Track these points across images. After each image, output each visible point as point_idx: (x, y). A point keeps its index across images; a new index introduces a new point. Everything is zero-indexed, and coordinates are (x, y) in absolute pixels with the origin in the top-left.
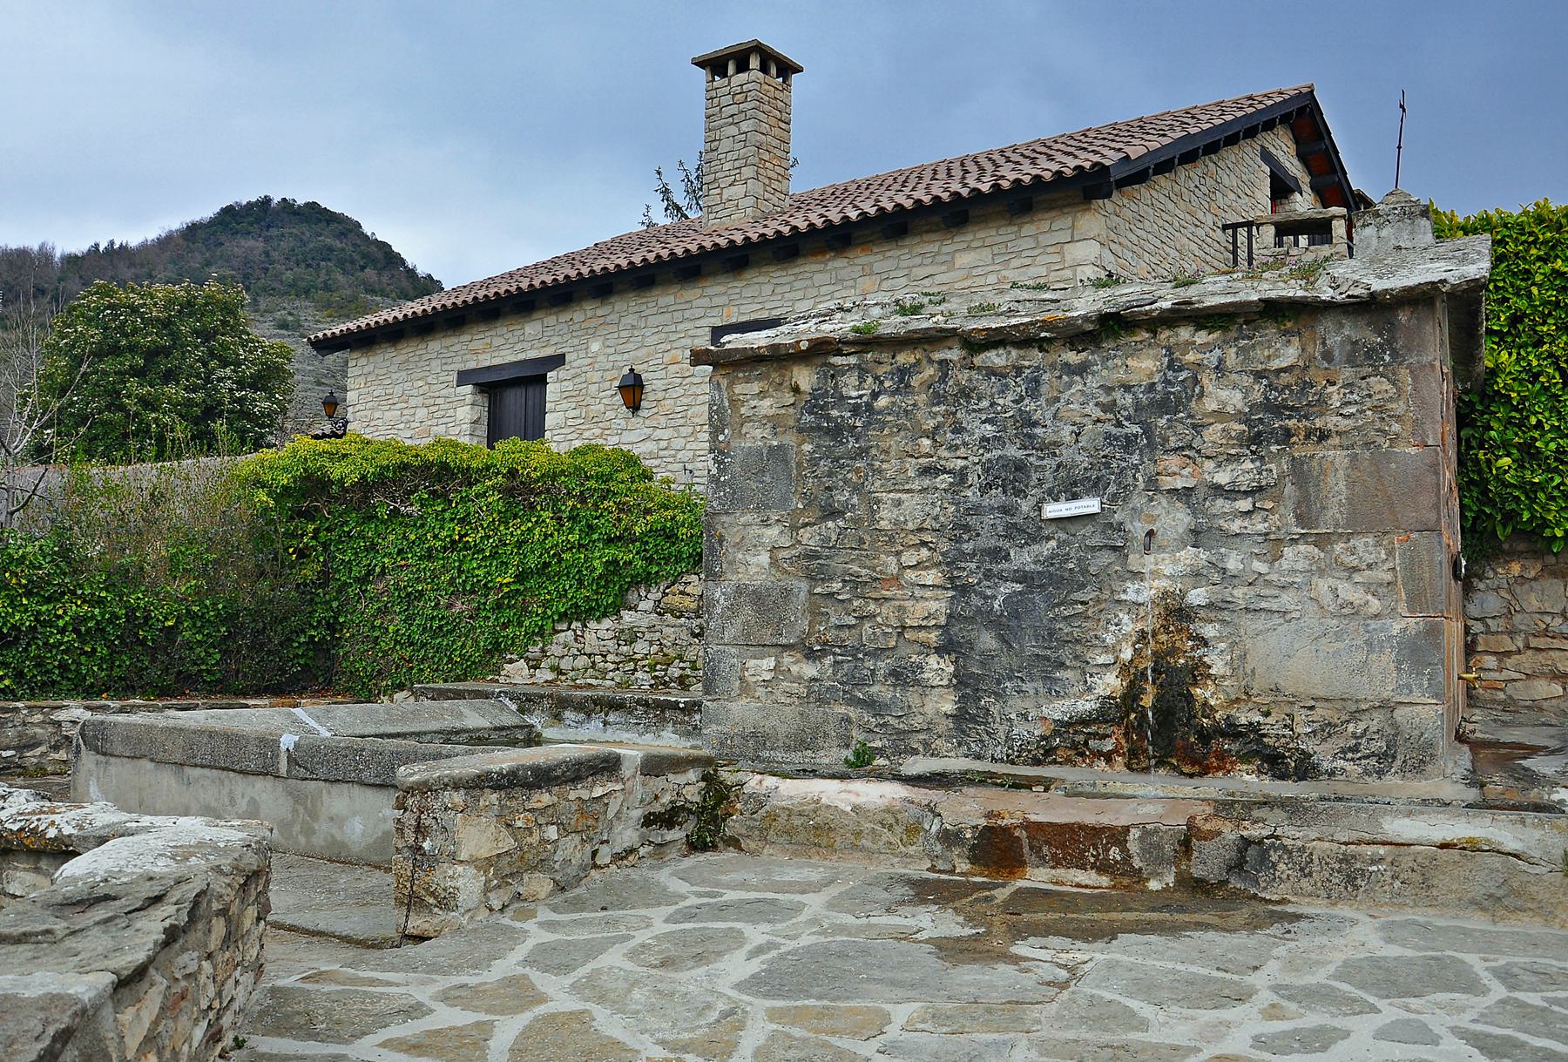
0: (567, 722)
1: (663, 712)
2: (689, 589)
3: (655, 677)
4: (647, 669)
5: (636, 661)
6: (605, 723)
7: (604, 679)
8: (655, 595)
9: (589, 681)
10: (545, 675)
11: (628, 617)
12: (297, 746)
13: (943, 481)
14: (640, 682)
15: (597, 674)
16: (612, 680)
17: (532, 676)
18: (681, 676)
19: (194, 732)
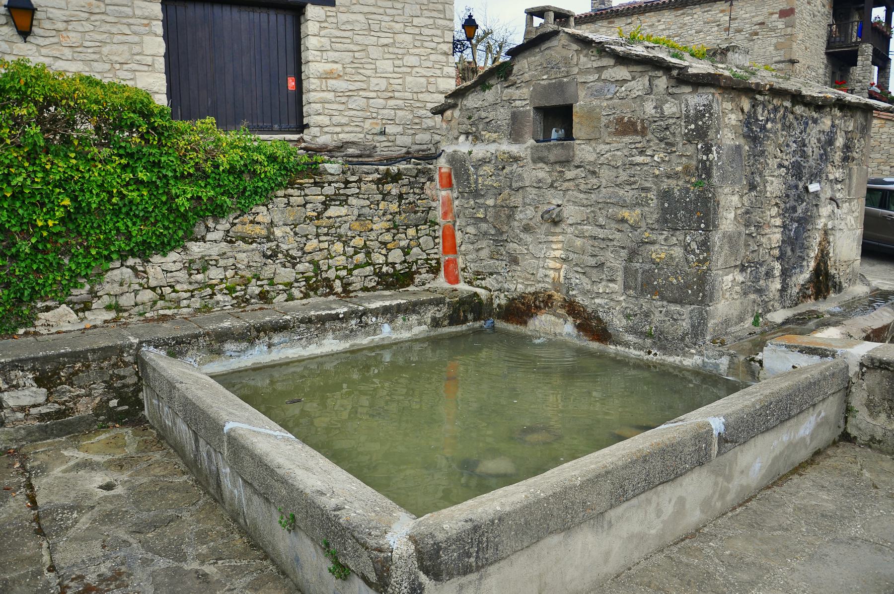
0: (228, 354)
1: (323, 324)
2: (259, 218)
3: (237, 297)
4: (225, 291)
5: (212, 286)
6: (270, 346)
7: (178, 307)
8: (224, 225)
9: (161, 312)
10: (98, 316)
11: (196, 249)
12: (727, 426)
13: (783, 171)
14: (221, 304)
15: (168, 304)
16: (188, 307)
17: (82, 320)
18: (261, 292)
19: (625, 467)
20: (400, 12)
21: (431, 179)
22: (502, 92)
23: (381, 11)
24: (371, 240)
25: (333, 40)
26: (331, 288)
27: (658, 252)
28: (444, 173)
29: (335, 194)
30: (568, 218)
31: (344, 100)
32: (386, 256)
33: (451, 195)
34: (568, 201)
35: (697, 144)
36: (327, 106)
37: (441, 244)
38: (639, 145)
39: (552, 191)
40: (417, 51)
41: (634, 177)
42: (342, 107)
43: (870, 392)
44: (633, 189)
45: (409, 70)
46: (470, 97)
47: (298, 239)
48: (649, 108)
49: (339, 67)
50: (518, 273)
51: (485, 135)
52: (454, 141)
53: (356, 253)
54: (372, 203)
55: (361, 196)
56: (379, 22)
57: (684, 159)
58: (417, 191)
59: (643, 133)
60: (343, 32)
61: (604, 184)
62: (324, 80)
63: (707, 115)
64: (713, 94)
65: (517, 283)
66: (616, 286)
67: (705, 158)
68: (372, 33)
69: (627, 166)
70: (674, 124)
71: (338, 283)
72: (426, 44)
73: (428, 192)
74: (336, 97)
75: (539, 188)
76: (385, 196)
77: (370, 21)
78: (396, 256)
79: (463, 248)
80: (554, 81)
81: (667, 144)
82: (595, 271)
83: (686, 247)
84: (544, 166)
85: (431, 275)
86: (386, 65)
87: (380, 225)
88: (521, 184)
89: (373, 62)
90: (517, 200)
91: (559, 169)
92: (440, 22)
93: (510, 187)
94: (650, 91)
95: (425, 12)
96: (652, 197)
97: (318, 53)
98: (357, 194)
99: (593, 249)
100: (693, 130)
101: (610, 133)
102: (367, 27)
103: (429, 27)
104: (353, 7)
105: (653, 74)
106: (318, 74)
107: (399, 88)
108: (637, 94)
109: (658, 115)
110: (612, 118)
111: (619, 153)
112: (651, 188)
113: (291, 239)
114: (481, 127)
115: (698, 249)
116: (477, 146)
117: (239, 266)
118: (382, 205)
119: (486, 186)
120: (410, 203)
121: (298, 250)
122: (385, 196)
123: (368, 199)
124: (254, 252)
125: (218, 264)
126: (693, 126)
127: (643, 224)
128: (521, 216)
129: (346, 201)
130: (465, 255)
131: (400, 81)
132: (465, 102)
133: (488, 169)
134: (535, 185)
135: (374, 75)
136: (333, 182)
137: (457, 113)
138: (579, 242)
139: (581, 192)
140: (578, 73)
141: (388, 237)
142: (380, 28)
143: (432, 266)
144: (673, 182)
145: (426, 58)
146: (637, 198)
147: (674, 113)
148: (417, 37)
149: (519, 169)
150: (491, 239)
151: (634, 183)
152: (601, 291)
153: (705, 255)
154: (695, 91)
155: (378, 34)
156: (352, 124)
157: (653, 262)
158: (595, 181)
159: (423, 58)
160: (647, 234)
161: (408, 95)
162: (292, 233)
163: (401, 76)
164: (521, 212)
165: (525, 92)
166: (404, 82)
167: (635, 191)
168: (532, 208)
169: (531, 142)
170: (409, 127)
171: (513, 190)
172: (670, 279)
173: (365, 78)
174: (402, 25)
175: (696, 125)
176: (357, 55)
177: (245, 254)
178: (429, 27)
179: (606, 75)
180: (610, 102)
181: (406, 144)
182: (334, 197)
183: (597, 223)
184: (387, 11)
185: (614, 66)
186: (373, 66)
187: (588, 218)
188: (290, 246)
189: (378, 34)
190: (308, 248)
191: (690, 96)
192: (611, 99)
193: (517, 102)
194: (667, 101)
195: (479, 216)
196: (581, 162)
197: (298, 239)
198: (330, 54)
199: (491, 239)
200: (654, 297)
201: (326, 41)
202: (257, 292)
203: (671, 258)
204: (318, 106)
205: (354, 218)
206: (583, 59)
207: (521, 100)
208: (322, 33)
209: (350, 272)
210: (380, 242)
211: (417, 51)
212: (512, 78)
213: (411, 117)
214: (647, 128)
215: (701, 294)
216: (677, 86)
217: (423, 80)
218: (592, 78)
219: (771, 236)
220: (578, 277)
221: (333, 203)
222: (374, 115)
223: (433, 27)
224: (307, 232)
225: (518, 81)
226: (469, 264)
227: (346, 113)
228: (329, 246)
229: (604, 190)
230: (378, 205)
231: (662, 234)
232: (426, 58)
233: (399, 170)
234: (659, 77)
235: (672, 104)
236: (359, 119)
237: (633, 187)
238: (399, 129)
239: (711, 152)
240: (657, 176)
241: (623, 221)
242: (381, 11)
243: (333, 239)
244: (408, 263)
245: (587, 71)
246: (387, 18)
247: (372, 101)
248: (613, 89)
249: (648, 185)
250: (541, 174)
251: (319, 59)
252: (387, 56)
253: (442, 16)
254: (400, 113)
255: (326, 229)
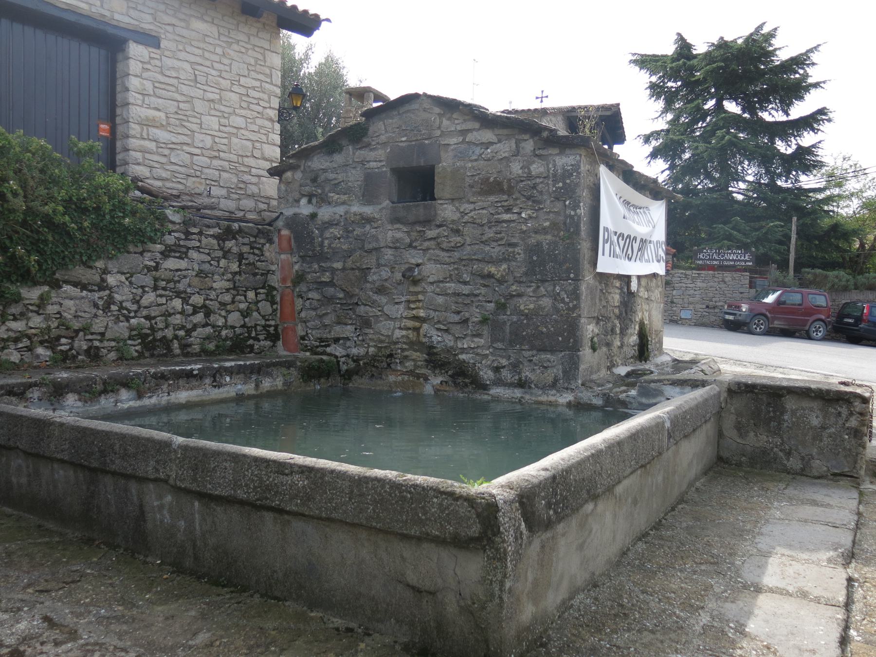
20: (227, 68)
21: (270, 241)
22: (354, 154)
23: (208, 63)
24: (211, 300)
25: (157, 85)
26: (169, 349)
27: (526, 304)
28: (284, 235)
29: (175, 245)
30: (429, 277)
31: (166, 152)
32: (225, 318)
33: (290, 259)
34: (429, 260)
35: (565, 201)
36: (147, 156)
37: (279, 311)
38: (506, 204)
39: (412, 251)
40: (243, 112)
41: (500, 233)
42: (163, 160)
43: (739, 414)
44: (499, 245)
45: (235, 131)
46: (315, 159)
47: (134, 291)
48: (516, 168)
49: (162, 115)
50: (370, 336)
51: (333, 197)
52: (295, 203)
53: (195, 312)
54: (213, 259)
55: (201, 250)
56: (205, 75)
57: (551, 215)
58: (256, 251)
59: (509, 193)
60: (167, 78)
61: (468, 240)
62: (145, 127)
63: (575, 174)
64: (580, 155)
65: (369, 346)
66: (482, 341)
67: (573, 213)
68: (198, 85)
69: (493, 224)
70: (542, 183)
71: (176, 344)
72: (252, 106)
73: (267, 254)
74: (158, 147)
75: (395, 248)
76: (226, 254)
77: (197, 72)
78: (234, 318)
79: (303, 315)
80: (414, 143)
81: (534, 201)
82: (458, 327)
83: (555, 297)
84: (401, 226)
85: (269, 342)
86: (212, 122)
87: (220, 284)
88: (374, 245)
89: (198, 116)
90: (370, 261)
91: (419, 229)
92: (267, 86)
93: (362, 248)
94: (517, 153)
95: (252, 73)
96: (520, 251)
97: (140, 97)
98: (197, 247)
99: (457, 305)
100: (561, 188)
101: (474, 194)
102: (193, 77)
103: (256, 89)
104: (179, 53)
105: (520, 137)
106: (139, 119)
107: (224, 148)
108: (504, 155)
109: (525, 175)
110: (477, 178)
111: (485, 212)
112: (518, 243)
113: (126, 290)
114: (327, 189)
115: (567, 297)
116: (323, 208)
117: (65, 314)
118: (223, 263)
119: (333, 249)
120: (249, 264)
121: (133, 304)
122: (226, 254)
123: (208, 254)
124: (83, 301)
125: (39, 311)
126: (561, 185)
127: (510, 279)
128: (375, 278)
129: (186, 253)
130: (305, 322)
131: (225, 141)
132: (310, 164)
133: (336, 231)
134: (391, 245)
135: (198, 130)
136: (174, 231)
137: (299, 175)
138: (440, 300)
139: (443, 250)
140: (440, 136)
141: (227, 298)
142: (207, 81)
143: (270, 333)
144: (540, 237)
145: (252, 121)
146: (503, 253)
147: (542, 173)
148: (244, 98)
149: (373, 230)
150: (338, 303)
151: (502, 239)
152: (465, 346)
153: (575, 302)
154: (561, 153)
155: (205, 88)
156: (174, 180)
157: (521, 313)
158: (459, 239)
159: (249, 120)
160: (514, 287)
161: (234, 158)
162: (127, 283)
163: (226, 135)
164: (375, 273)
165: (381, 153)
166: (230, 142)
167: (501, 247)
168: (387, 269)
169: (386, 203)
170: (233, 191)
171: (366, 251)
172: (540, 328)
173: (189, 133)
174: (229, 82)
175: (564, 183)
176: (182, 105)
177: (72, 302)
178: (256, 89)
179: (470, 137)
180: (475, 164)
181: (231, 209)
182: (173, 248)
183: (461, 280)
184: (215, 65)
185: (479, 129)
186: (199, 121)
187: (451, 275)
188: (124, 298)
189: (205, 88)
190: (144, 302)
191: (558, 157)
192: (476, 160)
193: (371, 163)
194: (534, 162)
195: (324, 280)
196: (444, 221)
197: (134, 291)
198: (153, 99)
199: (338, 303)
200: (523, 347)
201: (149, 85)
202: (85, 347)
203: (541, 308)
204: (138, 155)
205: (194, 273)
206: (445, 122)
207: (376, 161)
208: (145, 75)
209: (189, 332)
210: (220, 303)
211: (243, 112)
212: (365, 140)
213: (235, 180)
214: (513, 187)
215: (571, 340)
216: (544, 148)
217: (249, 144)
218: (453, 141)
219: (613, 295)
220: (440, 334)
221: (173, 254)
222: (198, 173)
223: (260, 90)
224: (144, 284)
225: (373, 143)
226: (310, 331)
227: (168, 167)
228: (167, 301)
229: (469, 248)
230: (218, 262)
231: (530, 286)
232: (252, 121)
233: (240, 227)
234: (526, 140)
235: (539, 165)
236: (182, 176)
237: (499, 243)
238: (224, 192)
239: (579, 207)
240: (524, 232)
241: (490, 276)
242: (208, 63)
243: (171, 294)
244: (248, 328)
245: (451, 134)
246: (214, 73)
247: (195, 158)
248: (478, 151)
249: (514, 241)
250: (399, 235)
251: (140, 102)
252: (213, 112)
253: (269, 80)
254: (225, 175)
255: (164, 283)
